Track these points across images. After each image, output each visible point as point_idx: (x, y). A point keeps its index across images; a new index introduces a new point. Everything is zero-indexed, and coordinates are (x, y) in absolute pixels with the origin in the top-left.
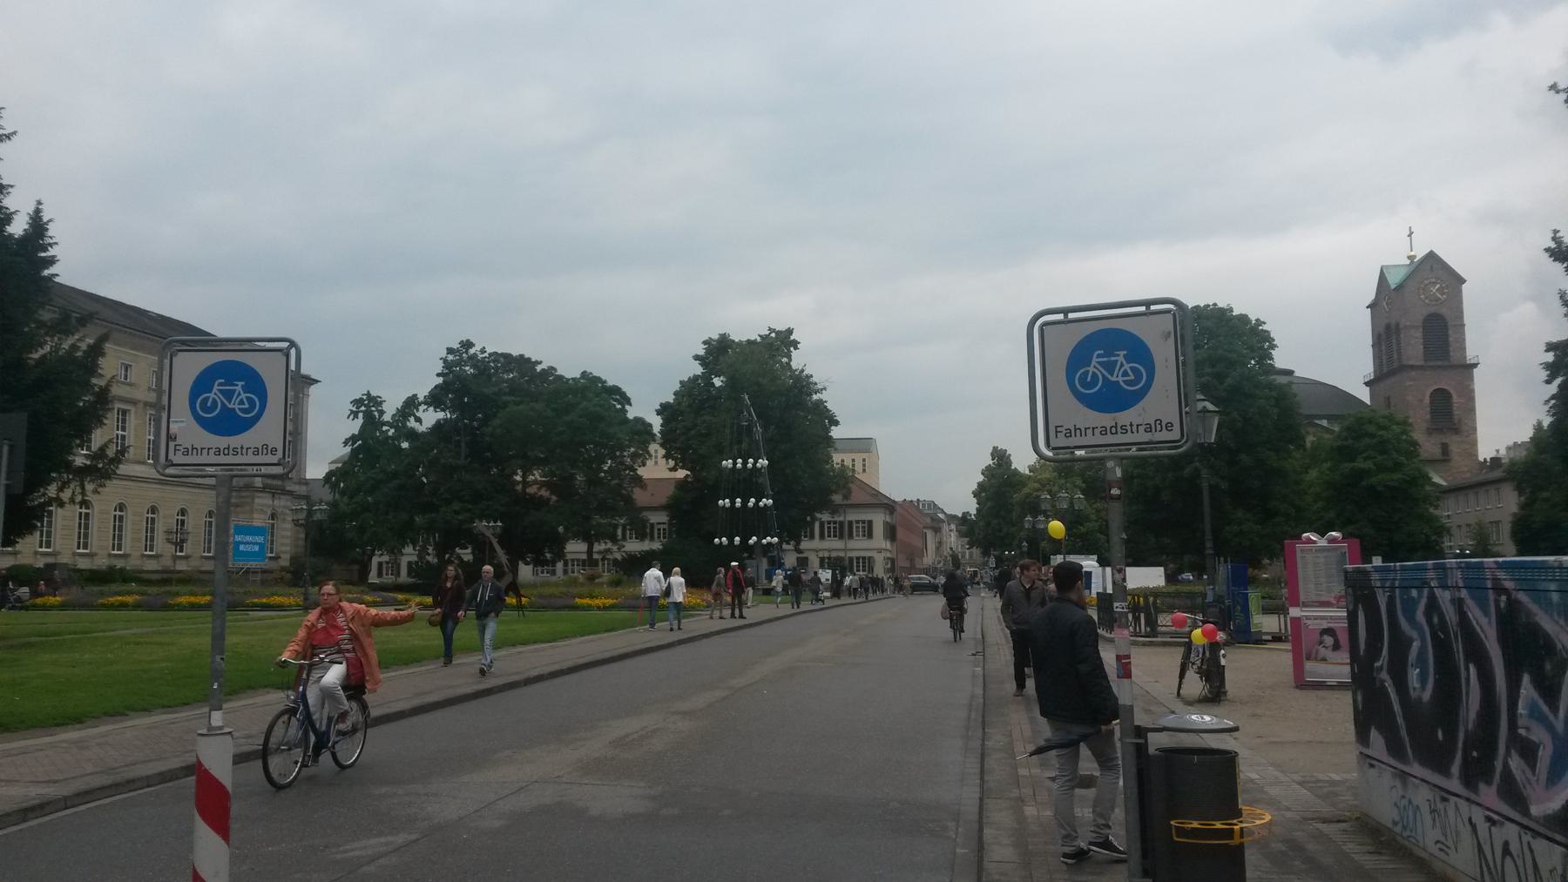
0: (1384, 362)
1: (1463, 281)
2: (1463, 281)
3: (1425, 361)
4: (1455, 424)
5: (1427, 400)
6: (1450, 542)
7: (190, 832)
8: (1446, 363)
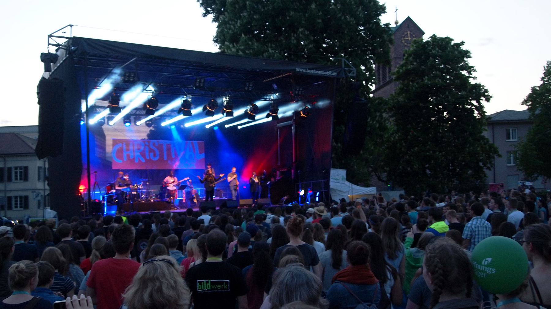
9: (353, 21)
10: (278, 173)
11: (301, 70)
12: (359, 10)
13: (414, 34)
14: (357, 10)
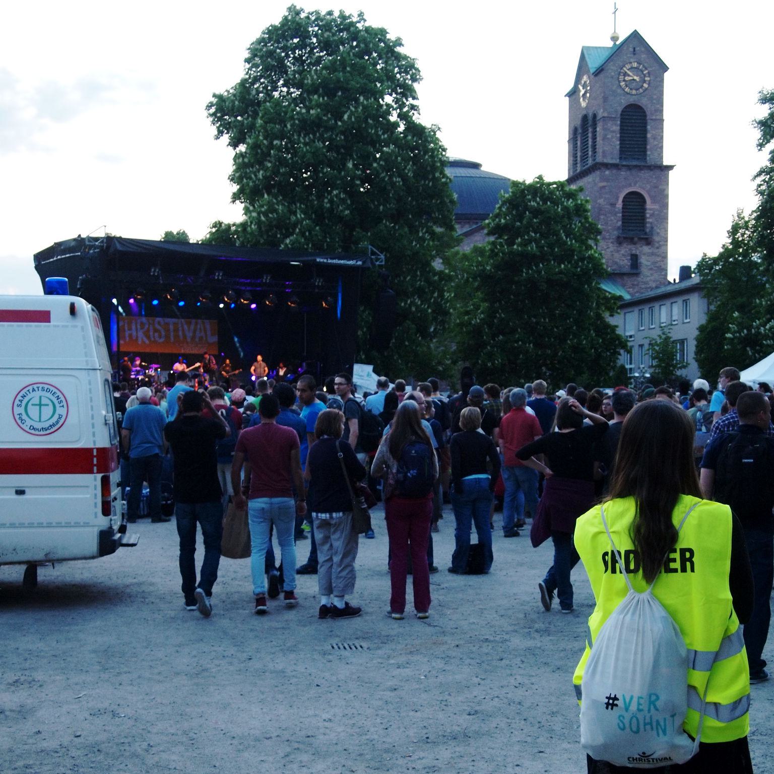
0: (579, 159)
1: (665, 68)
2: (665, 68)
3: (620, 158)
4: (646, 234)
5: (620, 205)
6: (631, 364)
7: (742, 647)
8: (643, 164)
9: (399, 182)
10: (304, 364)
11: (322, 260)
12: (408, 168)
13: (646, 69)
14: (406, 168)
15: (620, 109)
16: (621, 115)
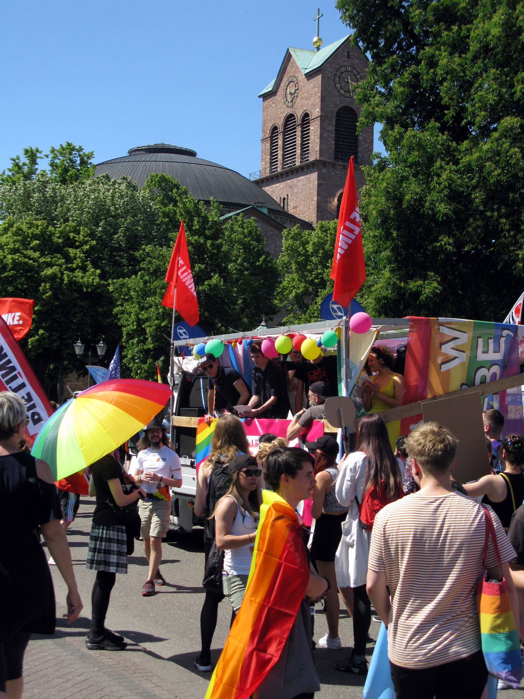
15: (336, 110)
16: (336, 116)
